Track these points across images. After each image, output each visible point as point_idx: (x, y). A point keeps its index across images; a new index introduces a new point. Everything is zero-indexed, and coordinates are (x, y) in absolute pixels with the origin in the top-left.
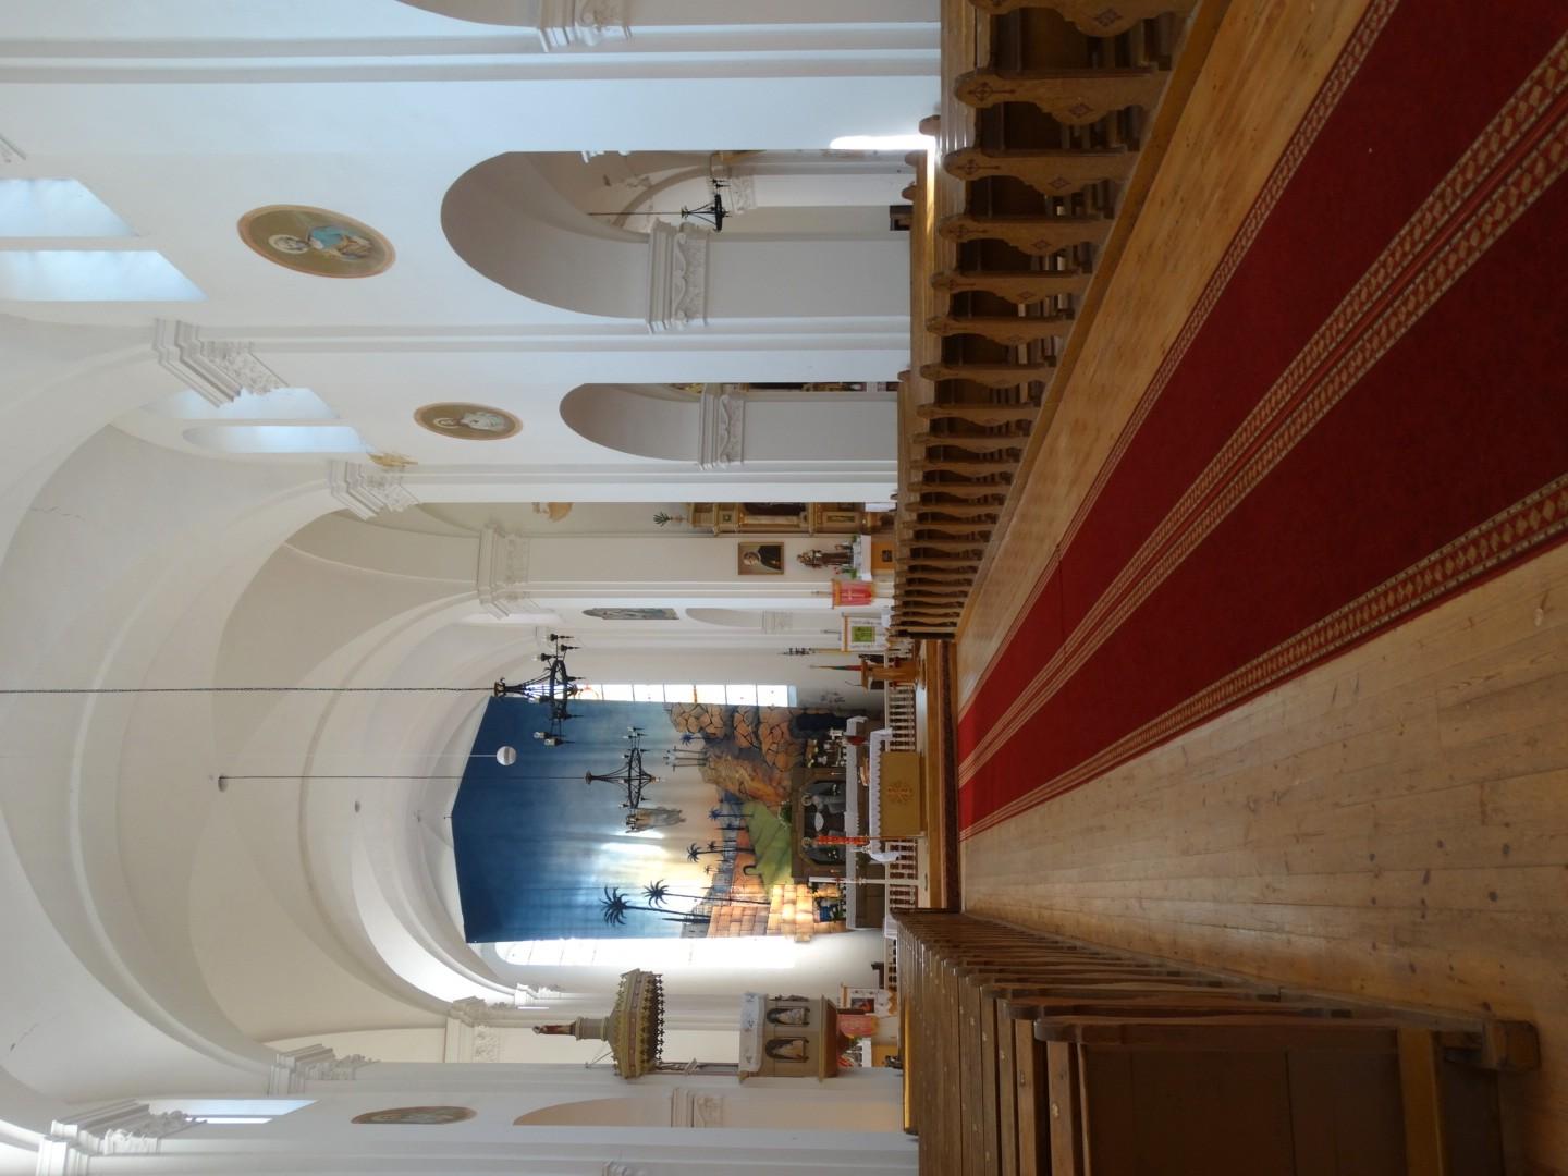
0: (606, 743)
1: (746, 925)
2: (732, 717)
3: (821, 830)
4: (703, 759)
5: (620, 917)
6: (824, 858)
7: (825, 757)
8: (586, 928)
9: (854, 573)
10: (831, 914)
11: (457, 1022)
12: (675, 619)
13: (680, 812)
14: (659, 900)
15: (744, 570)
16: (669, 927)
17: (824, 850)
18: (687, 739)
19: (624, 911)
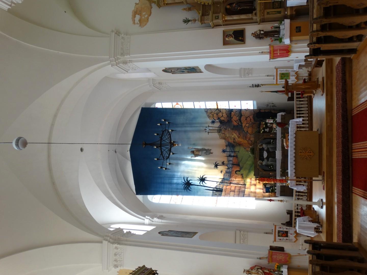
0: (183, 124)
1: (236, 193)
2: (231, 113)
3: (266, 158)
4: (219, 130)
5: (189, 188)
6: (267, 169)
7: (268, 129)
8: (177, 192)
9: (280, 40)
10: (270, 190)
11: (107, 242)
12: (201, 72)
13: (211, 150)
14: (203, 183)
15: (225, 43)
16: (208, 193)
17: (267, 166)
18: (213, 122)
19: (190, 186)
